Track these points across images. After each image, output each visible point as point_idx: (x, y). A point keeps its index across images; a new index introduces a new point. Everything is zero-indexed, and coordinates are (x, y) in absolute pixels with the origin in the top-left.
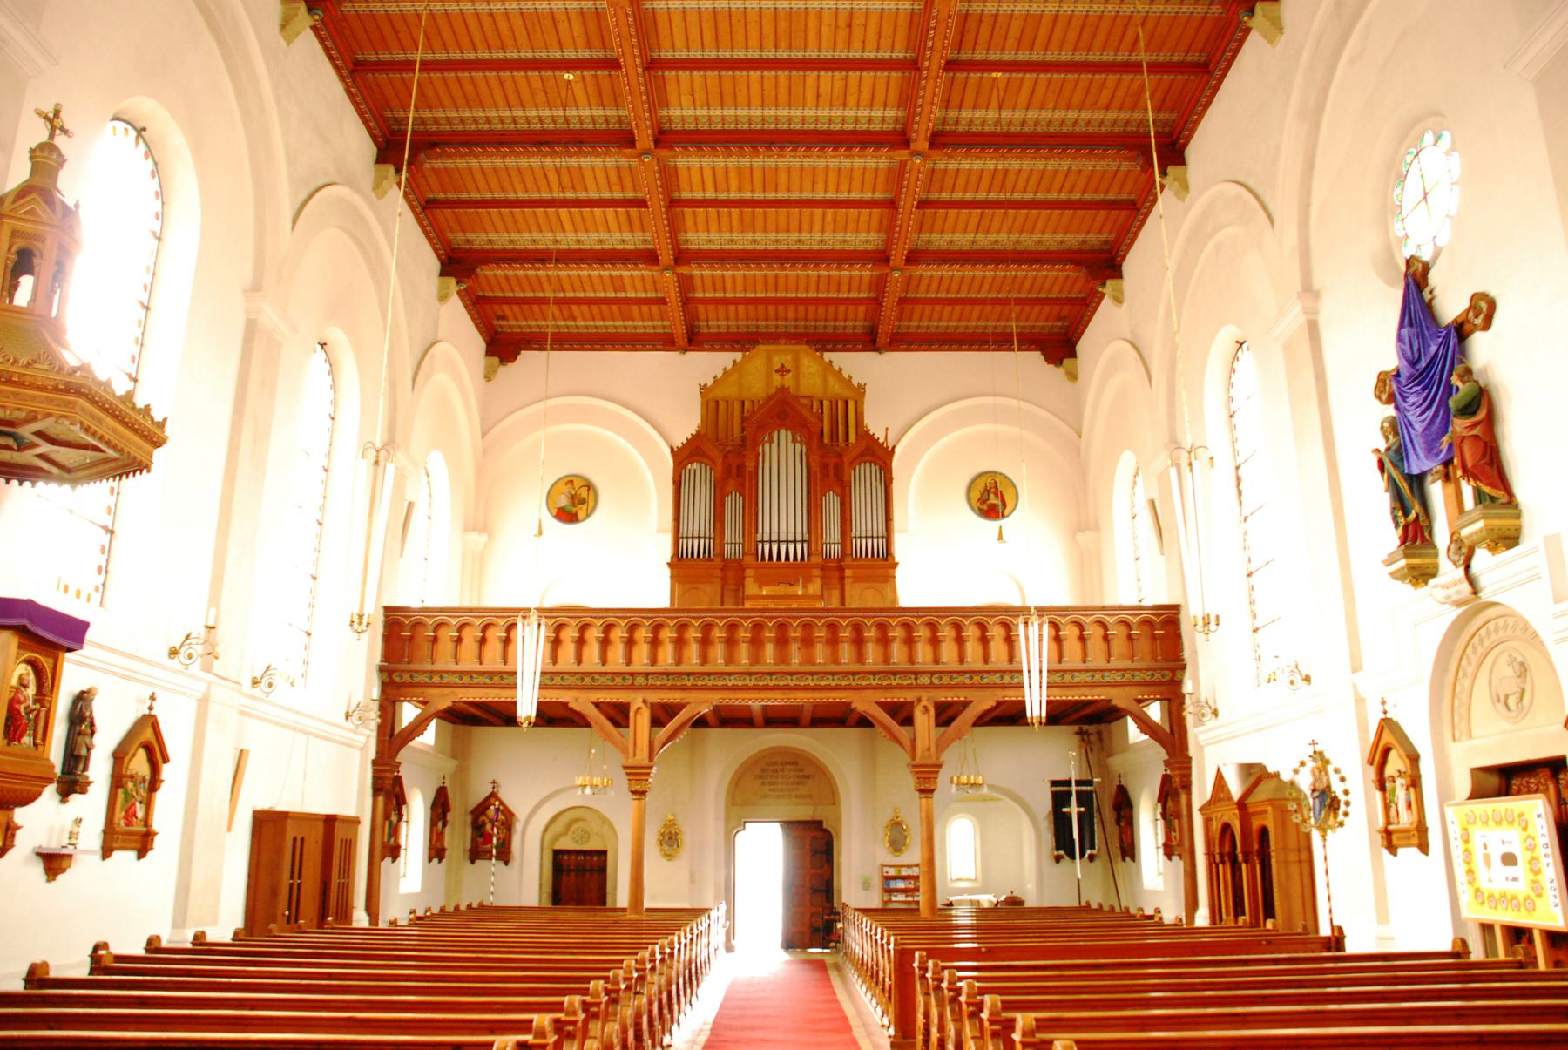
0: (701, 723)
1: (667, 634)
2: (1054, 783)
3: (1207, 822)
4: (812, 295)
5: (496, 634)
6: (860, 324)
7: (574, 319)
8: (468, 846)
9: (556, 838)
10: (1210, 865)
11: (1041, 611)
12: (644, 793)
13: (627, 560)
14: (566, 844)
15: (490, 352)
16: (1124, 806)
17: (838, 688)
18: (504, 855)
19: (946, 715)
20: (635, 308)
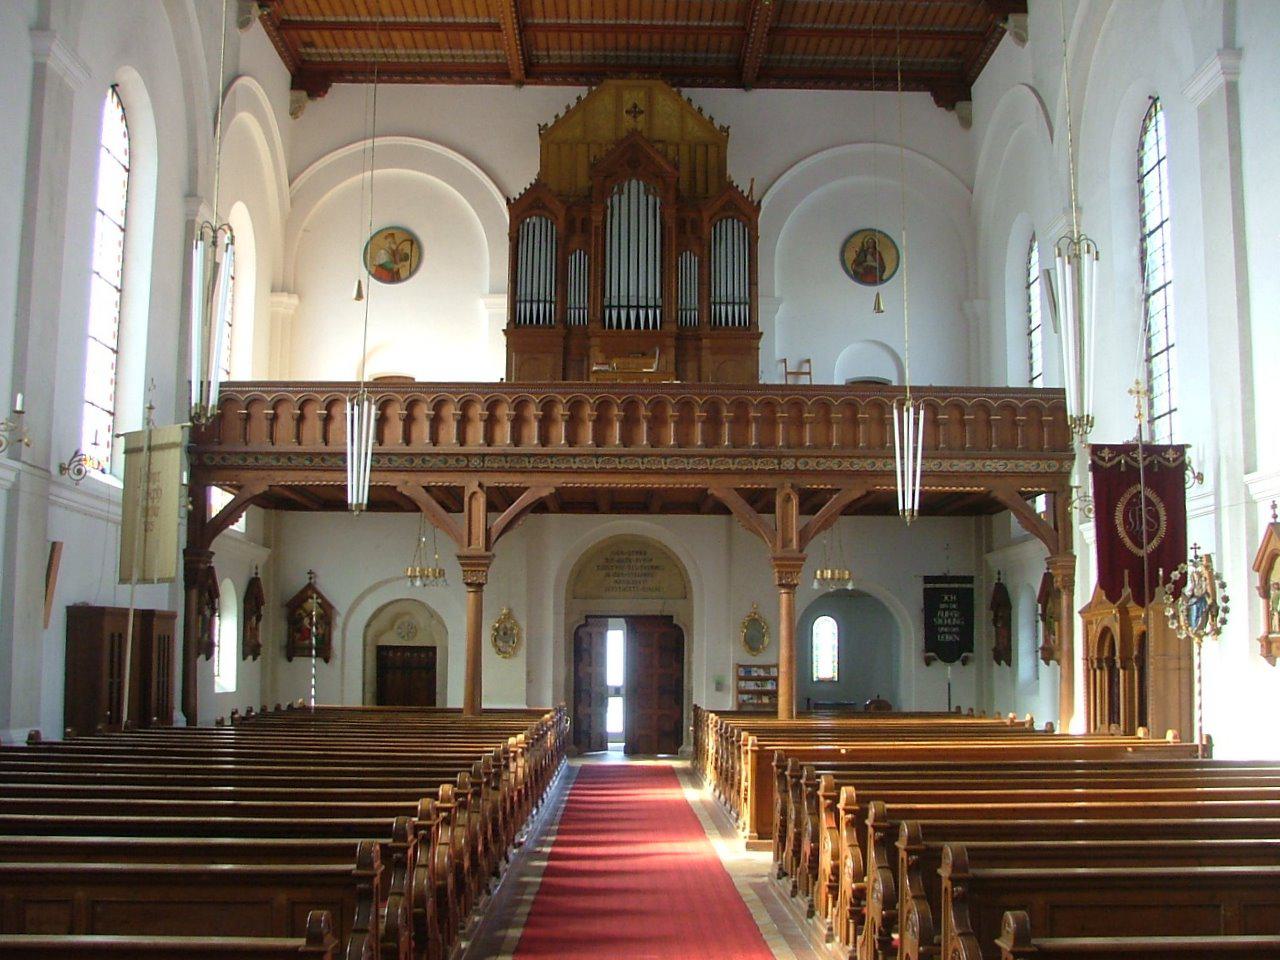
0: (540, 507)
1: (505, 412)
2: (927, 579)
3: (1087, 625)
4: (670, 22)
5: (316, 411)
6: (723, 55)
7: (394, 47)
8: (284, 640)
9: (380, 634)
10: (1088, 671)
11: (917, 391)
12: (480, 585)
13: (454, 332)
14: (391, 639)
15: (297, 83)
16: (1002, 605)
17: (694, 472)
18: (325, 652)
19: (810, 502)
20: (464, 35)
